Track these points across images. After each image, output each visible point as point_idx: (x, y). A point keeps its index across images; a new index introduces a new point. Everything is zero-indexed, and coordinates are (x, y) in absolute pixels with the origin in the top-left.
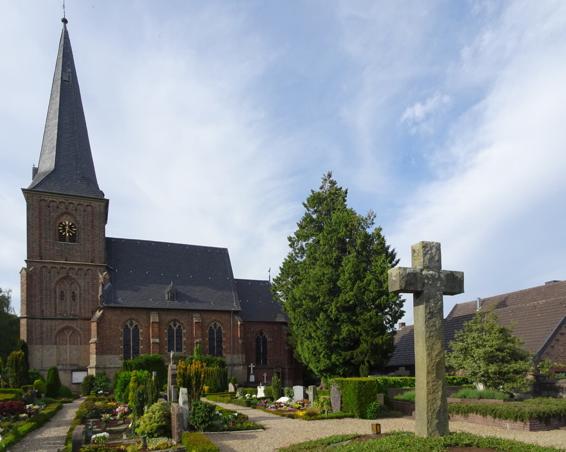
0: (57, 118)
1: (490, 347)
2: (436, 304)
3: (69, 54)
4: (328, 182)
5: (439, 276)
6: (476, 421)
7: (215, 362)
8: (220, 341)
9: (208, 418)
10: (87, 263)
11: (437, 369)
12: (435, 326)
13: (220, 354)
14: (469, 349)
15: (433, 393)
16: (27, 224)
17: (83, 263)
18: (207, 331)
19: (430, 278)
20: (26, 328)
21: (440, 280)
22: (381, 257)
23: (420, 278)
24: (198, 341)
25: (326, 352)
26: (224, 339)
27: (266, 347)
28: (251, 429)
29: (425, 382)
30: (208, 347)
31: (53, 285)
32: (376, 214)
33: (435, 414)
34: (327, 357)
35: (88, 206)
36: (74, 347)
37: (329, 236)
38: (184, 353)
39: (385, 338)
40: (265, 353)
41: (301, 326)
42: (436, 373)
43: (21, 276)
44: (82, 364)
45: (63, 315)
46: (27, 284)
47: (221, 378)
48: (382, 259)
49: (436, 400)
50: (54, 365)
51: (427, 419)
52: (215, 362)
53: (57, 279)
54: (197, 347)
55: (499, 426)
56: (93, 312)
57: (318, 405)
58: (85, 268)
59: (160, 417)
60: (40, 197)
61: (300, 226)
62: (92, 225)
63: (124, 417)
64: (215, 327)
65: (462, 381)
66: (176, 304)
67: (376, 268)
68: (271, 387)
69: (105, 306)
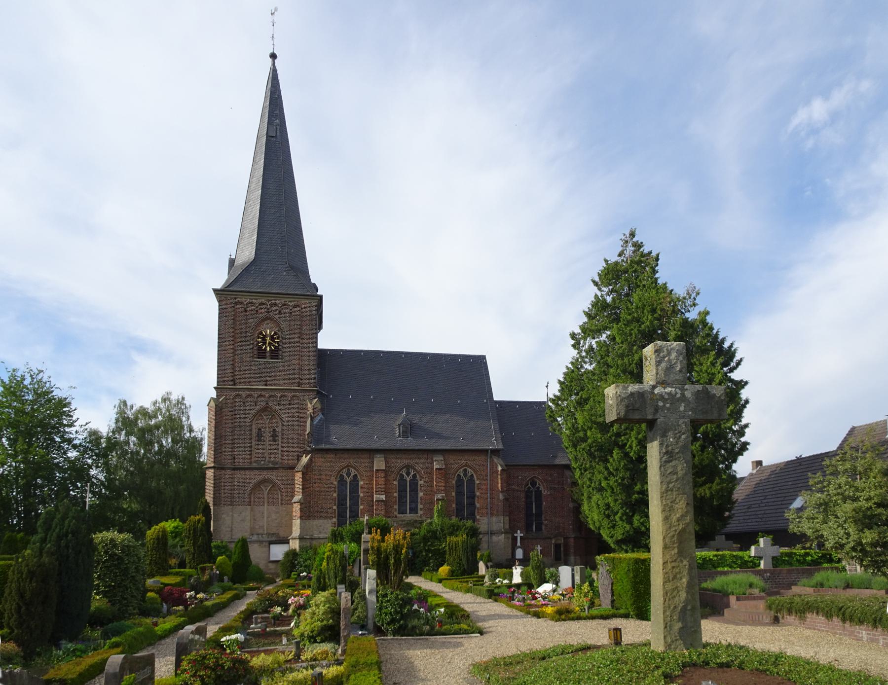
0: (260, 188)
1: (867, 500)
2: (678, 439)
3: (277, 99)
4: (630, 244)
5: (683, 395)
6: (817, 626)
7: (464, 529)
8: (472, 497)
9: (399, 615)
10: (293, 388)
11: (680, 542)
12: (676, 473)
13: (472, 516)
14: (832, 505)
15: (673, 580)
16: (219, 337)
17: (288, 388)
18: (454, 482)
19: (667, 400)
20: (212, 482)
21: (683, 401)
22: (708, 357)
23: (651, 399)
24: (439, 496)
25: (625, 511)
26: (478, 494)
27: (541, 504)
28: (463, 634)
29: (661, 562)
30: (454, 505)
31: (248, 420)
32: (699, 290)
33: (677, 613)
34: (626, 519)
35: (295, 306)
36: (273, 508)
37: (628, 328)
38: (421, 515)
39: (715, 487)
40: (539, 514)
41: (585, 471)
42: (678, 547)
43: (209, 409)
44: (282, 534)
45: (260, 463)
46: (216, 420)
47: (467, 553)
48: (710, 360)
49: (678, 592)
50: (246, 535)
51: (664, 621)
52: (464, 529)
53: (253, 412)
54: (438, 506)
55: (851, 634)
56: (299, 458)
57: (580, 597)
58: (290, 395)
59: (325, 612)
60: (235, 298)
61: (588, 315)
62: (301, 333)
63: (298, 612)
64: (465, 475)
65: (820, 558)
66: (410, 443)
67: (700, 376)
68: (529, 568)
69: (314, 449)
